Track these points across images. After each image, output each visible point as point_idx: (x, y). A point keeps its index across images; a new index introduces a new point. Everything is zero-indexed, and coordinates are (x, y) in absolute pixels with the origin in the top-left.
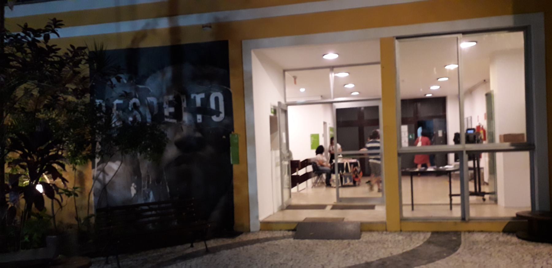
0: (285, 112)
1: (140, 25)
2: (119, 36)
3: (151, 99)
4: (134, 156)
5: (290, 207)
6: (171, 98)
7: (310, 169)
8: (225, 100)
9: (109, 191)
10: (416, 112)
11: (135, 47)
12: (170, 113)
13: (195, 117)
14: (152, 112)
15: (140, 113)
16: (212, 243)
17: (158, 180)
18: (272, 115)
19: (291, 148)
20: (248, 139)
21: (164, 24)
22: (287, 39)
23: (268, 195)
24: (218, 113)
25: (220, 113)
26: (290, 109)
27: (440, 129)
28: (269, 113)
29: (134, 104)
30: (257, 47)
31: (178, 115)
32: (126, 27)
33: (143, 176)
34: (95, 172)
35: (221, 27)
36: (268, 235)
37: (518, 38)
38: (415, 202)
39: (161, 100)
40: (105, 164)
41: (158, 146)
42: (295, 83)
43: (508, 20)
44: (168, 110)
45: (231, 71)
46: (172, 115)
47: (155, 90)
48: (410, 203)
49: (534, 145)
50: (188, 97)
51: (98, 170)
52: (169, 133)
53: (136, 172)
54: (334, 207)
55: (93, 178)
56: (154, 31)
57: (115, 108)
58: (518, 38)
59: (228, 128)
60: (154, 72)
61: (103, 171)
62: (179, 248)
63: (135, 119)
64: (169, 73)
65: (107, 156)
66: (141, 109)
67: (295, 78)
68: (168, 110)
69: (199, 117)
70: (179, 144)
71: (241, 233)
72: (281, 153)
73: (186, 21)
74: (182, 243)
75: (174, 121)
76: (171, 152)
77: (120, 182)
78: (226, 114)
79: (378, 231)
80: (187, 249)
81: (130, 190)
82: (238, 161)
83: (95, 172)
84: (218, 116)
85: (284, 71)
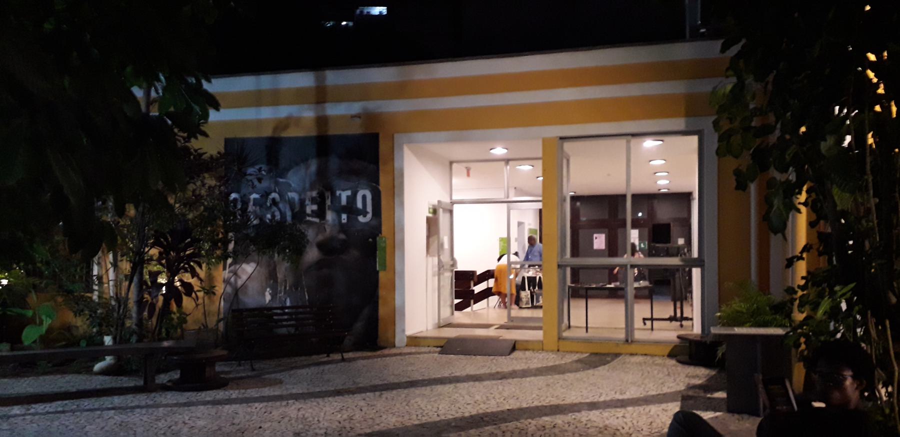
0: (451, 212)
2: (259, 123)
4: (272, 257)
5: (449, 325)
8: (373, 199)
9: (241, 296)
10: (651, 214)
11: (276, 136)
12: (312, 211)
14: (292, 209)
15: (279, 210)
16: (350, 355)
17: (296, 285)
18: (431, 215)
20: (396, 244)
21: (308, 113)
22: (443, 134)
24: (364, 213)
25: (368, 213)
26: (456, 208)
27: (681, 237)
28: (425, 213)
29: (274, 199)
30: (410, 142)
31: (320, 214)
32: (267, 113)
34: (226, 274)
35: (369, 117)
36: (413, 350)
37: (694, 140)
39: (303, 197)
40: (238, 266)
41: (297, 247)
42: (468, 175)
43: (680, 123)
44: (310, 208)
45: (381, 167)
46: (314, 214)
47: (297, 183)
50: (333, 194)
52: (311, 234)
53: (272, 275)
54: (501, 327)
57: (251, 203)
58: (694, 140)
59: (375, 230)
60: (297, 164)
61: (235, 273)
62: (314, 357)
64: (313, 166)
65: (240, 256)
66: (281, 205)
67: (468, 170)
68: (310, 208)
69: (344, 217)
70: (321, 246)
71: (385, 348)
73: (334, 110)
75: (317, 220)
76: (312, 254)
77: (253, 287)
78: (373, 215)
79: (533, 350)
81: (264, 295)
82: (384, 267)
83: (226, 274)
84: (365, 216)
85: (451, 163)
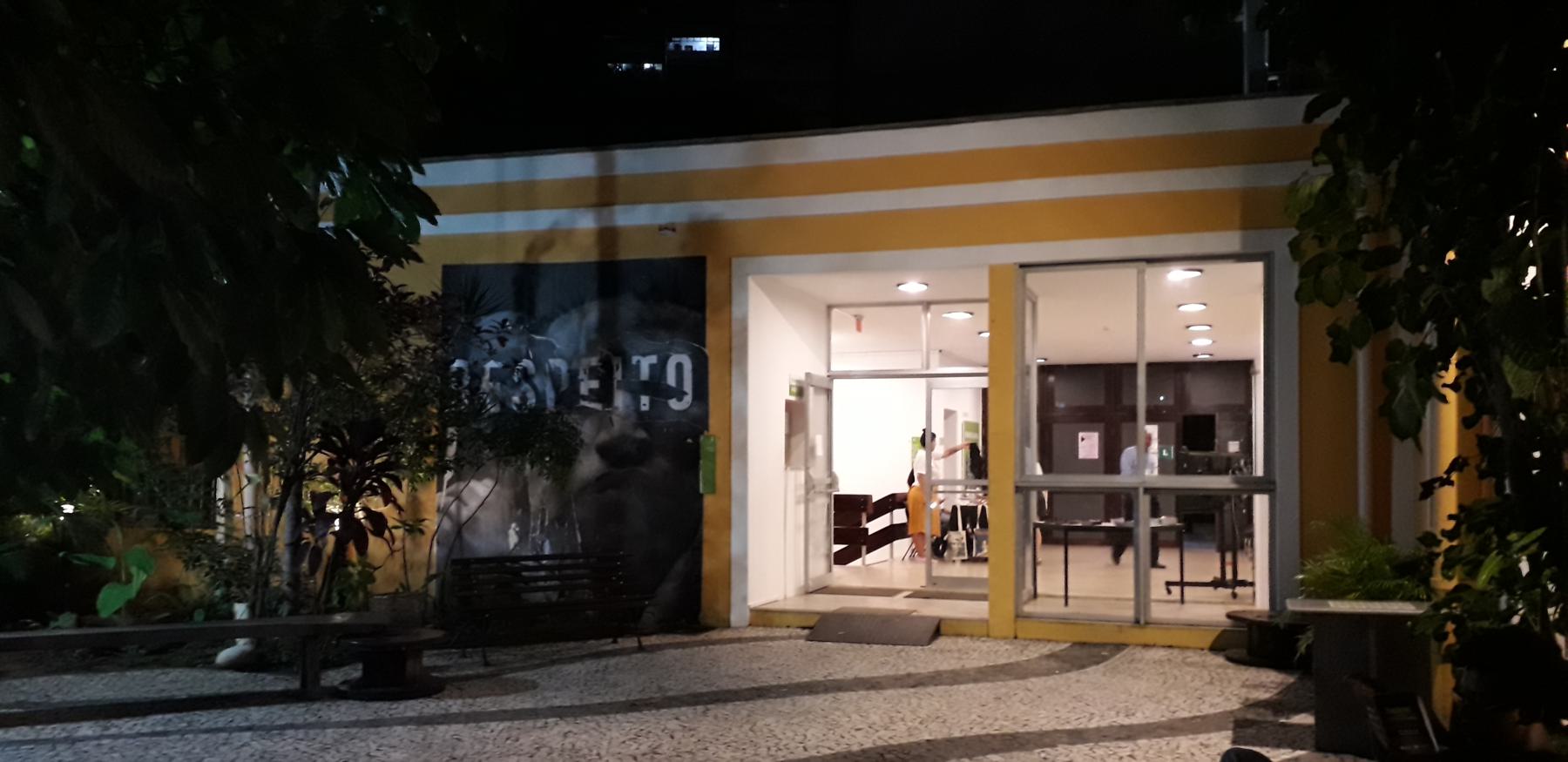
1: (543, 220)
2: (502, 239)
3: (557, 363)
4: (520, 470)
5: (825, 590)
6: (594, 361)
7: (899, 516)
8: (695, 371)
9: (467, 536)
10: (1181, 397)
12: (591, 391)
13: (638, 402)
14: (556, 387)
15: (534, 388)
16: (654, 640)
17: (561, 518)
19: (836, 469)
20: (734, 449)
21: (586, 222)
23: (773, 554)
24: (679, 394)
31: (604, 395)
32: (514, 222)
33: (532, 509)
34: (442, 498)
36: (761, 632)
37: (1255, 272)
38: (1070, 593)
39: (574, 365)
40: (462, 485)
41: (564, 452)
42: (859, 328)
43: (1231, 240)
44: (588, 385)
46: (595, 395)
47: (565, 342)
48: (1062, 593)
49: (1274, 483)
50: (626, 362)
51: (448, 495)
52: (587, 429)
53: (520, 501)
54: (916, 595)
55: (438, 510)
56: (570, 233)
57: (487, 376)
59: (697, 423)
60: (565, 311)
61: (458, 497)
63: (524, 399)
64: (593, 314)
65: (467, 467)
66: (537, 381)
68: (588, 385)
69: (645, 400)
70: (604, 451)
71: (712, 628)
72: (808, 478)
74: (598, 638)
75: (597, 406)
76: (589, 465)
77: (488, 520)
78: (695, 397)
79: (972, 636)
80: (606, 645)
81: (506, 536)
83: (442, 498)
84: (680, 400)
85: (830, 307)
